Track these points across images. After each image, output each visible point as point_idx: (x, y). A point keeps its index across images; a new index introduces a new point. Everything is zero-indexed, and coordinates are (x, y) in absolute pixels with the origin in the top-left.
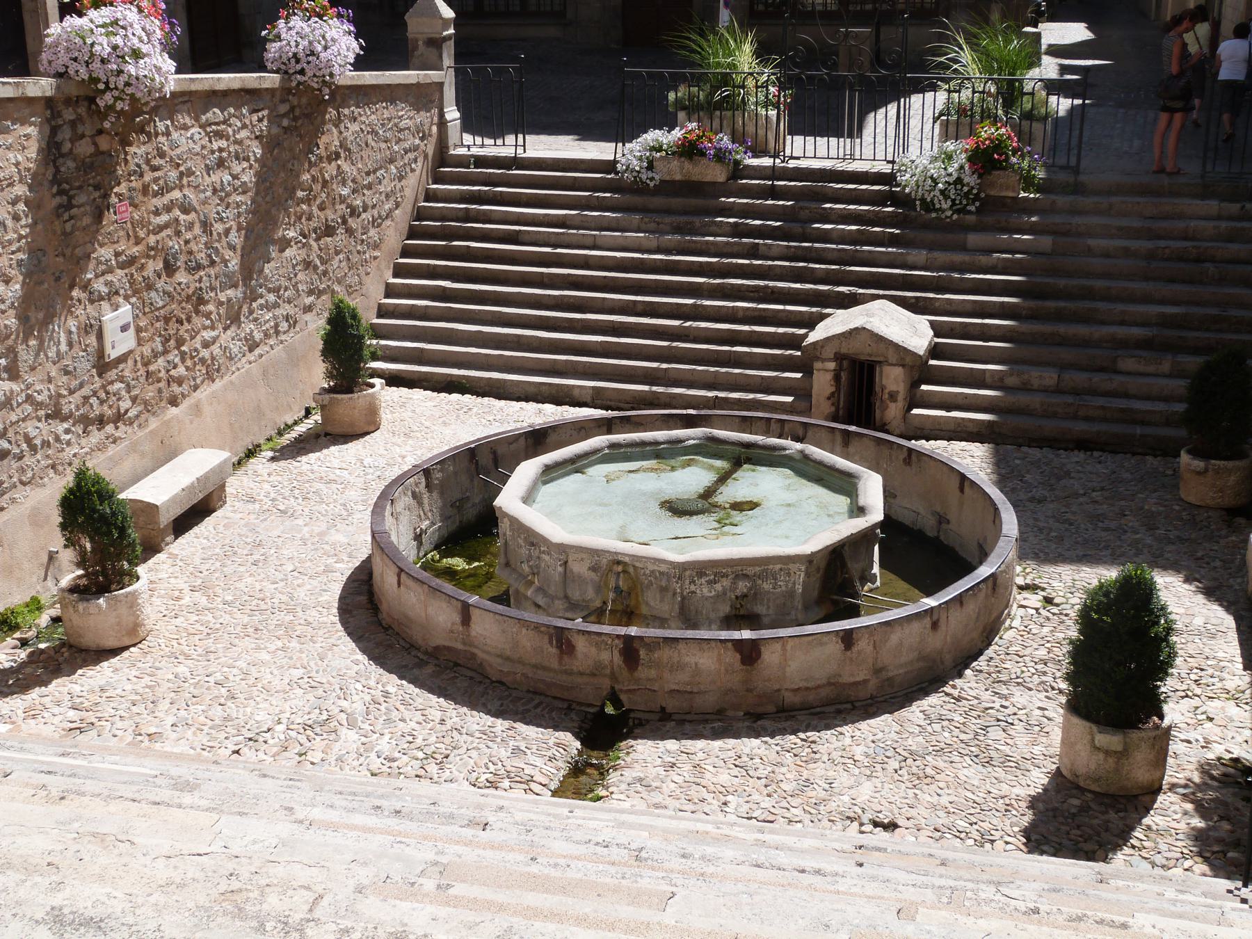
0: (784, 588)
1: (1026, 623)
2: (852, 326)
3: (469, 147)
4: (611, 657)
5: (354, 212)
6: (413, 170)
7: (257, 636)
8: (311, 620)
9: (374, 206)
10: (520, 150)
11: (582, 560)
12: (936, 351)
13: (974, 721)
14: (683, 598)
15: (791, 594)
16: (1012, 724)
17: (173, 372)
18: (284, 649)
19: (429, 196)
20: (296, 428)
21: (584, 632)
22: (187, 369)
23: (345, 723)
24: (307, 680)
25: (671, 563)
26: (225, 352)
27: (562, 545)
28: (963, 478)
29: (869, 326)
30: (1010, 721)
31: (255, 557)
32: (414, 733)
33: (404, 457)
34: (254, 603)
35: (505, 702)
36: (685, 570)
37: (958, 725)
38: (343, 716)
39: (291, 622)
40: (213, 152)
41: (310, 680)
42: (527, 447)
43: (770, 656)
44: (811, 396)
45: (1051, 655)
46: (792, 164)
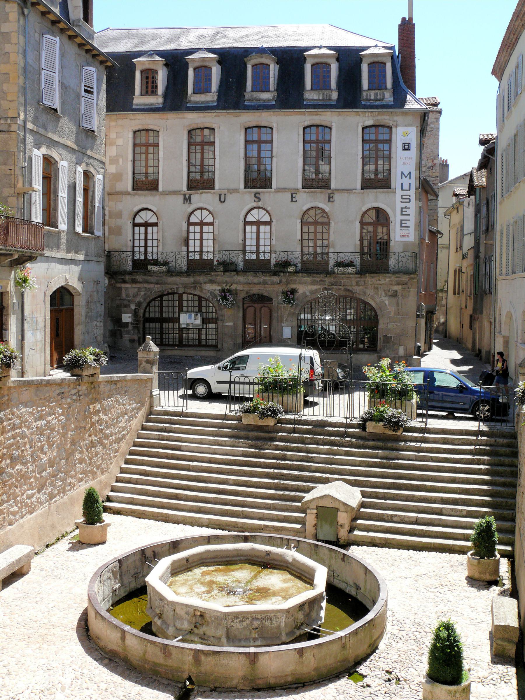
0: (275, 624)
1: (391, 641)
2: (324, 494)
3: (163, 406)
4: (189, 659)
5: (107, 437)
6: (136, 417)
7: (28, 641)
8: (56, 633)
9: (116, 434)
10: (185, 409)
11: (182, 609)
12: (363, 505)
13: (360, 694)
14: (228, 629)
15: (279, 627)
16: (377, 696)
17: (11, 510)
18: (40, 648)
19: (144, 428)
20: (71, 534)
21: (176, 647)
22: (19, 508)
23: (59, 689)
24: (46, 665)
25: (222, 612)
26: (38, 500)
27: (172, 602)
28: (366, 569)
29: (331, 494)
30: (376, 694)
31: (37, 599)
32: (91, 696)
33: (116, 550)
34: (31, 623)
35: (138, 680)
36: (228, 616)
37: (351, 696)
38: (60, 685)
39: (46, 634)
40: (38, 412)
41: (48, 666)
42: (169, 549)
43: (263, 661)
44: (305, 524)
45: (400, 658)
46: (304, 418)
